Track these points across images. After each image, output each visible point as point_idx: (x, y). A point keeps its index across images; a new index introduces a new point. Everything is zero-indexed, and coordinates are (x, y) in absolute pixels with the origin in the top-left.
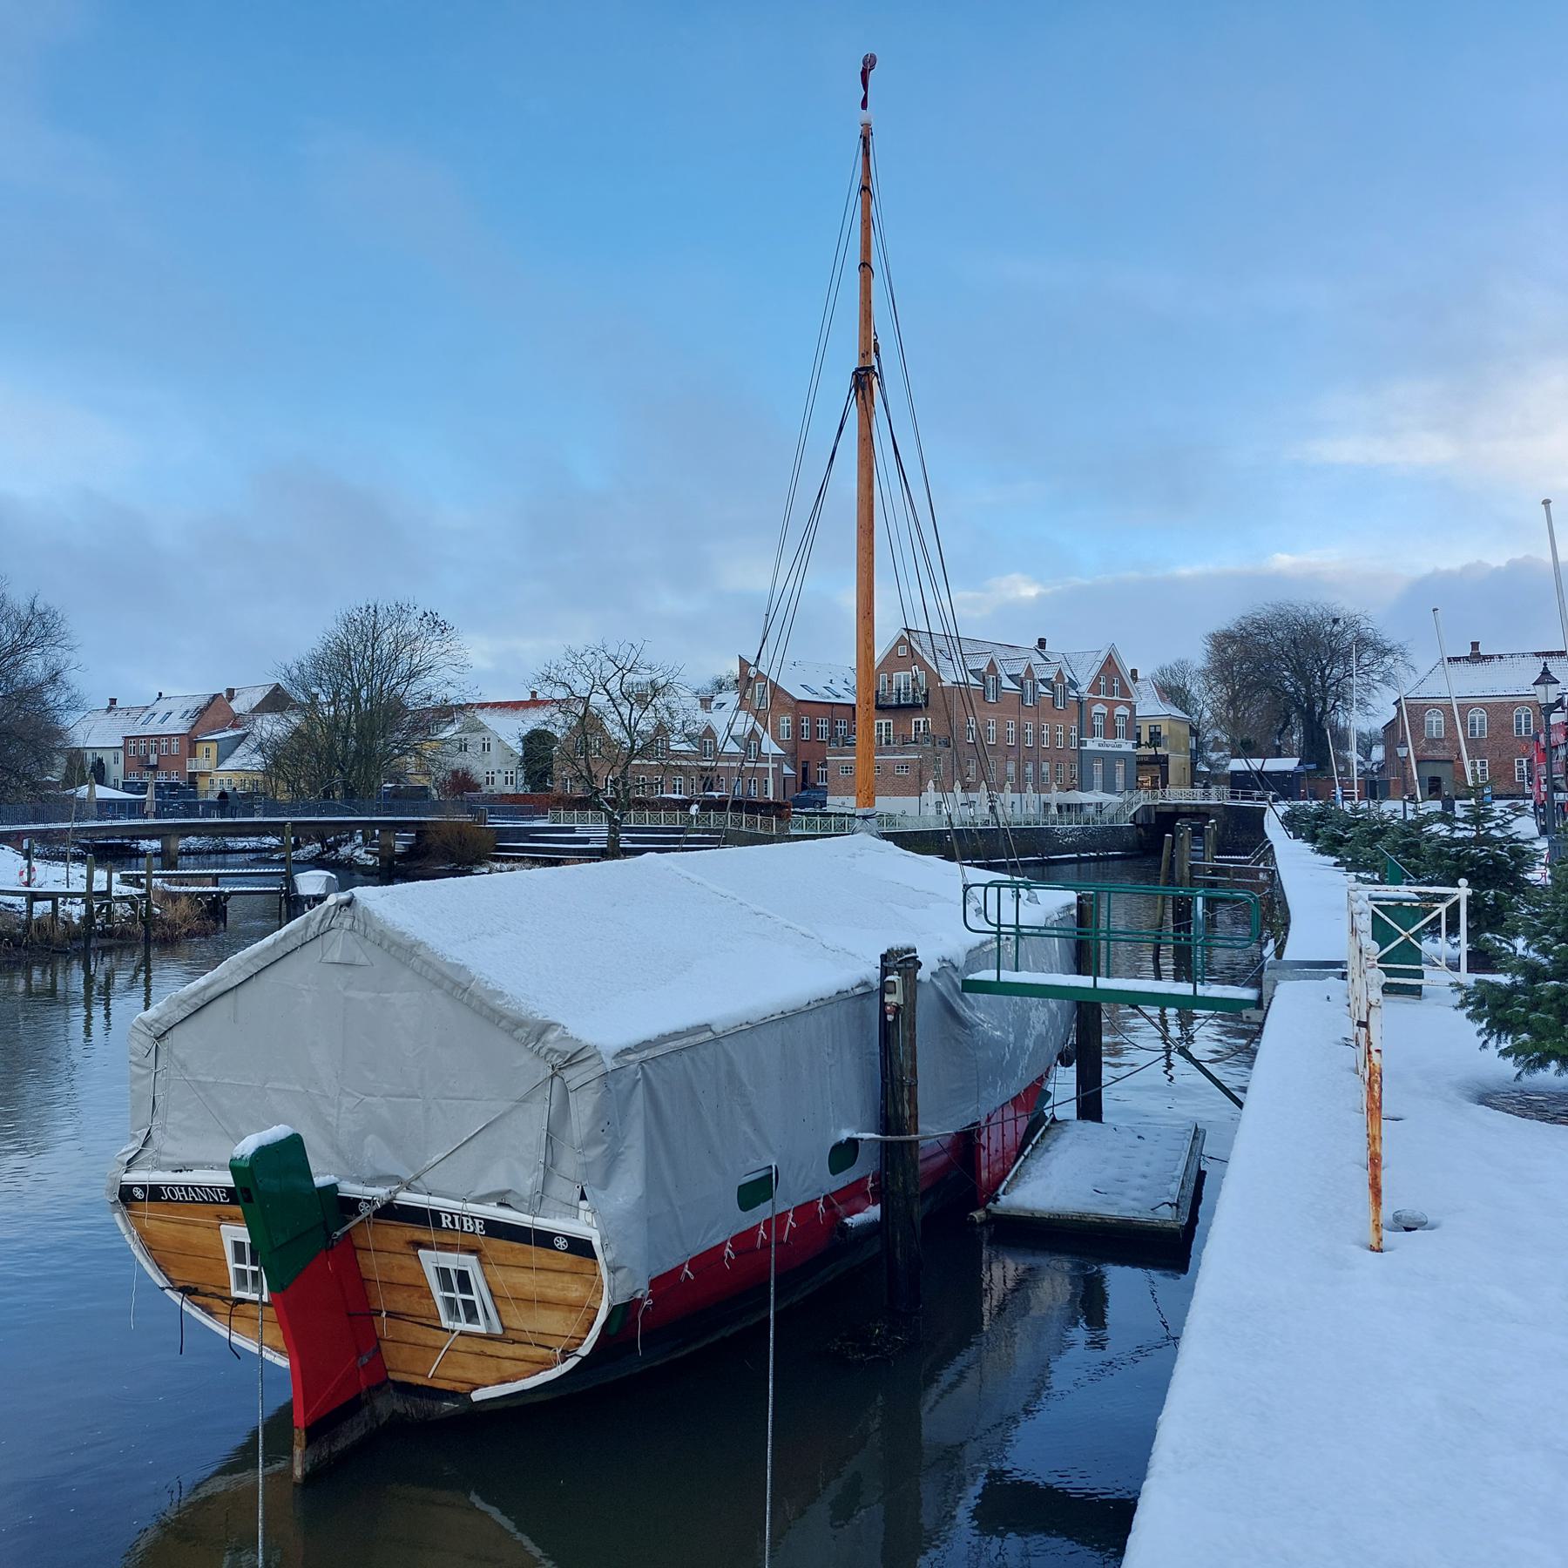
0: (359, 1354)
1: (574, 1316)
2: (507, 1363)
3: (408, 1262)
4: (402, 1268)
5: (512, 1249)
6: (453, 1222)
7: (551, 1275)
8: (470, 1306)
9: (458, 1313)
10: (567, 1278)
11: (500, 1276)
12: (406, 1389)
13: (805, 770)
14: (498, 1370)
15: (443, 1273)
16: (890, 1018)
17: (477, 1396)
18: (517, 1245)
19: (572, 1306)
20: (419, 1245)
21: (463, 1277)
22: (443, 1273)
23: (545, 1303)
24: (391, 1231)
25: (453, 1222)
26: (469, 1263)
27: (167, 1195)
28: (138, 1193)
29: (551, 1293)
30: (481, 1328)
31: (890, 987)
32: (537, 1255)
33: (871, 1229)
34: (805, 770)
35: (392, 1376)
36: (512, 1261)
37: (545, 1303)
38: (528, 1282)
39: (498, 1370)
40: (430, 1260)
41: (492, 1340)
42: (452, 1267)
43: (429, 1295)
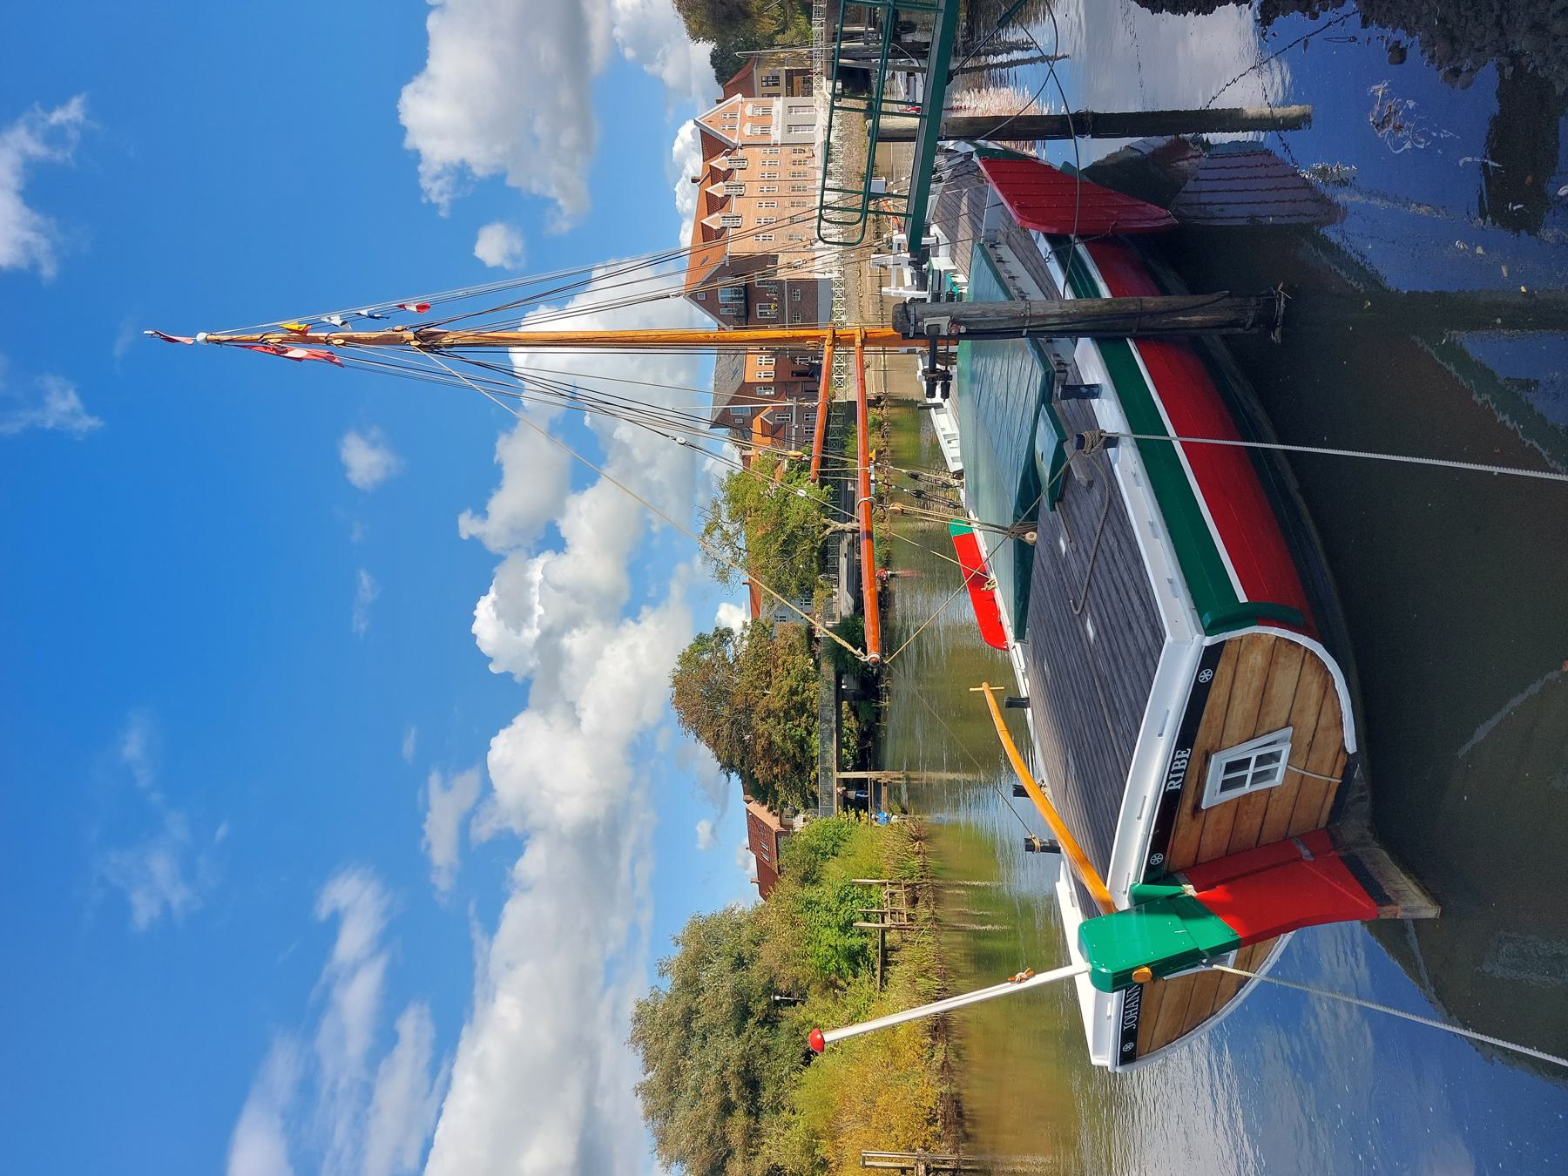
0: (1300, 859)
1: (1281, 660)
2: (1323, 721)
3: (1212, 818)
4: (1218, 822)
5: (1208, 721)
6: (1176, 779)
7: (1237, 684)
8: (1261, 760)
9: (1267, 772)
10: (1241, 668)
11: (1234, 730)
12: (1338, 810)
13: (800, 374)
14: (1328, 729)
15: (1226, 785)
16: (963, 329)
17: (1351, 747)
18: (1205, 717)
19: (1271, 662)
20: (1196, 808)
21: (1231, 767)
22: (1226, 785)
23: (1265, 690)
24: (1181, 832)
25: (1176, 779)
26: (1217, 763)
27: (1176, 786)
28: (1129, 1047)
29: (1256, 683)
30: (1285, 751)
31: (933, 330)
32: (1217, 696)
33: (1081, 635)
34: (800, 374)
35: (1322, 825)
36: (1220, 722)
37: (1265, 690)
38: (1243, 705)
39: (1328, 729)
40: (1213, 796)
41: (1302, 721)
42: (1221, 777)
43: (1248, 797)
